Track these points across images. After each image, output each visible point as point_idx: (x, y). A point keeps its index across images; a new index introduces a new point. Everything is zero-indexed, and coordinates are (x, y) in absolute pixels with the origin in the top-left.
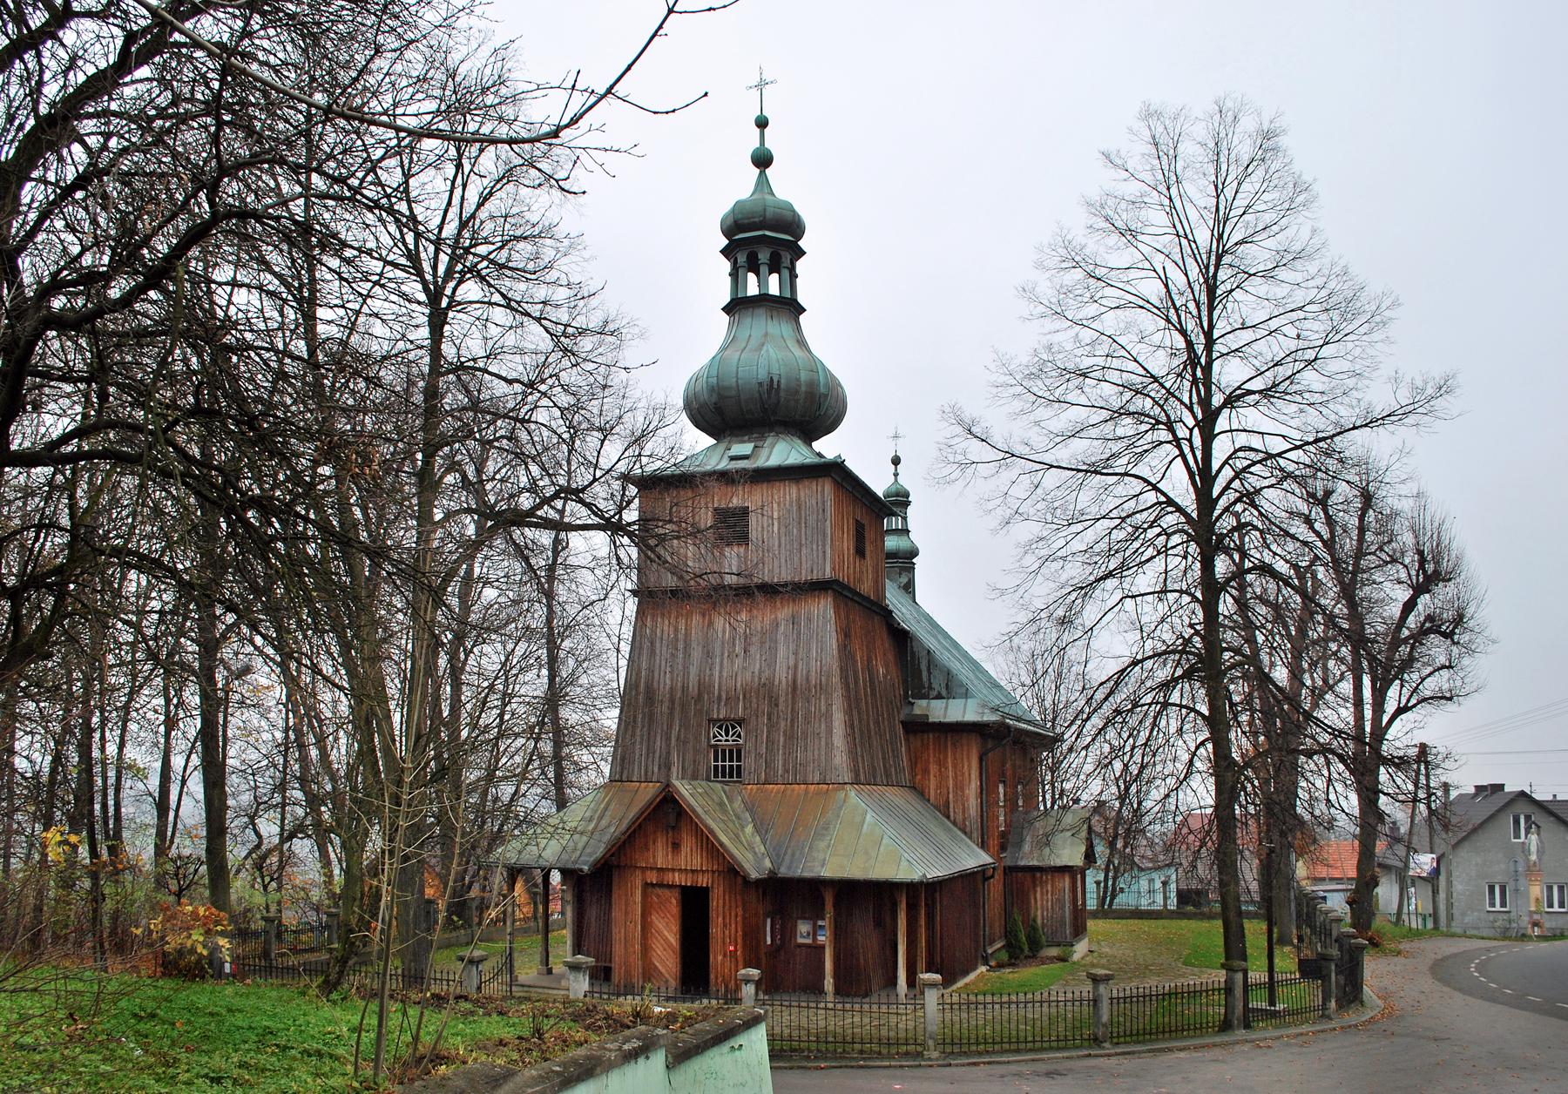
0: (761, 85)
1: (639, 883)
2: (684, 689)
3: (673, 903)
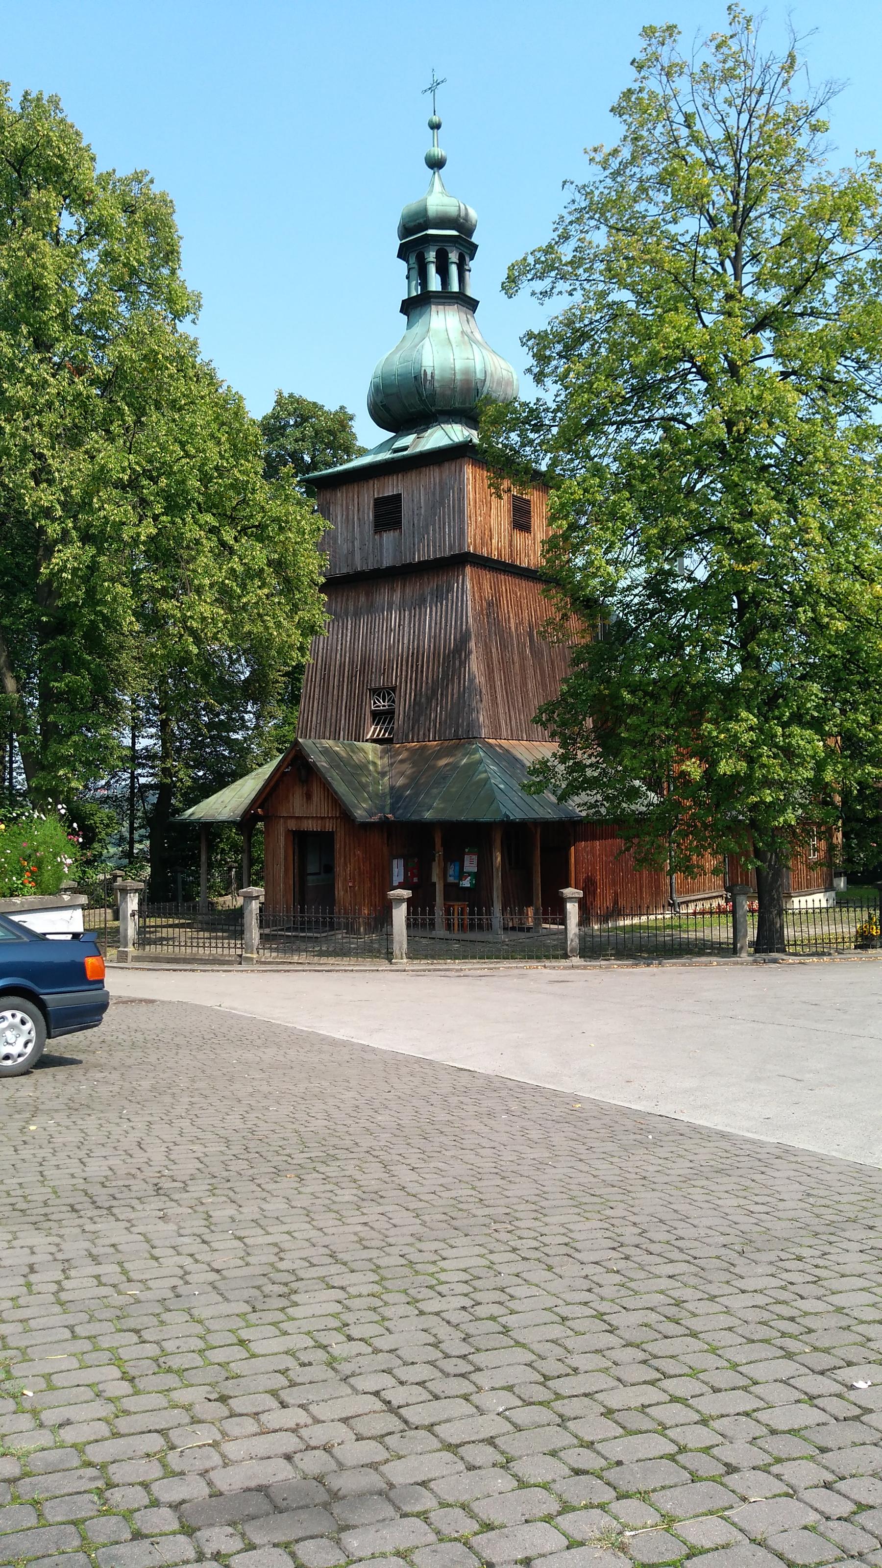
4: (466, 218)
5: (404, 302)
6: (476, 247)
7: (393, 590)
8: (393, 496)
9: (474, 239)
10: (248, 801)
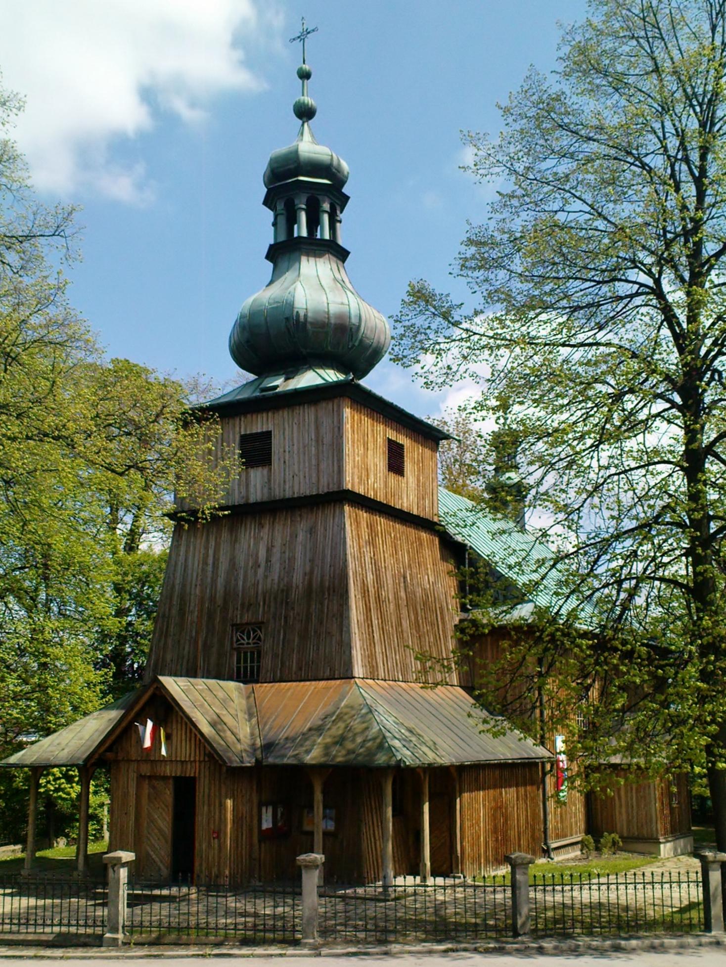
0: (302, 37)
1: (133, 775)
2: (212, 599)
3: (168, 794)
4: (339, 169)
5: (271, 246)
6: (346, 198)
7: (261, 526)
8: (262, 433)
9: (346, 190)
10: (97, 743)
